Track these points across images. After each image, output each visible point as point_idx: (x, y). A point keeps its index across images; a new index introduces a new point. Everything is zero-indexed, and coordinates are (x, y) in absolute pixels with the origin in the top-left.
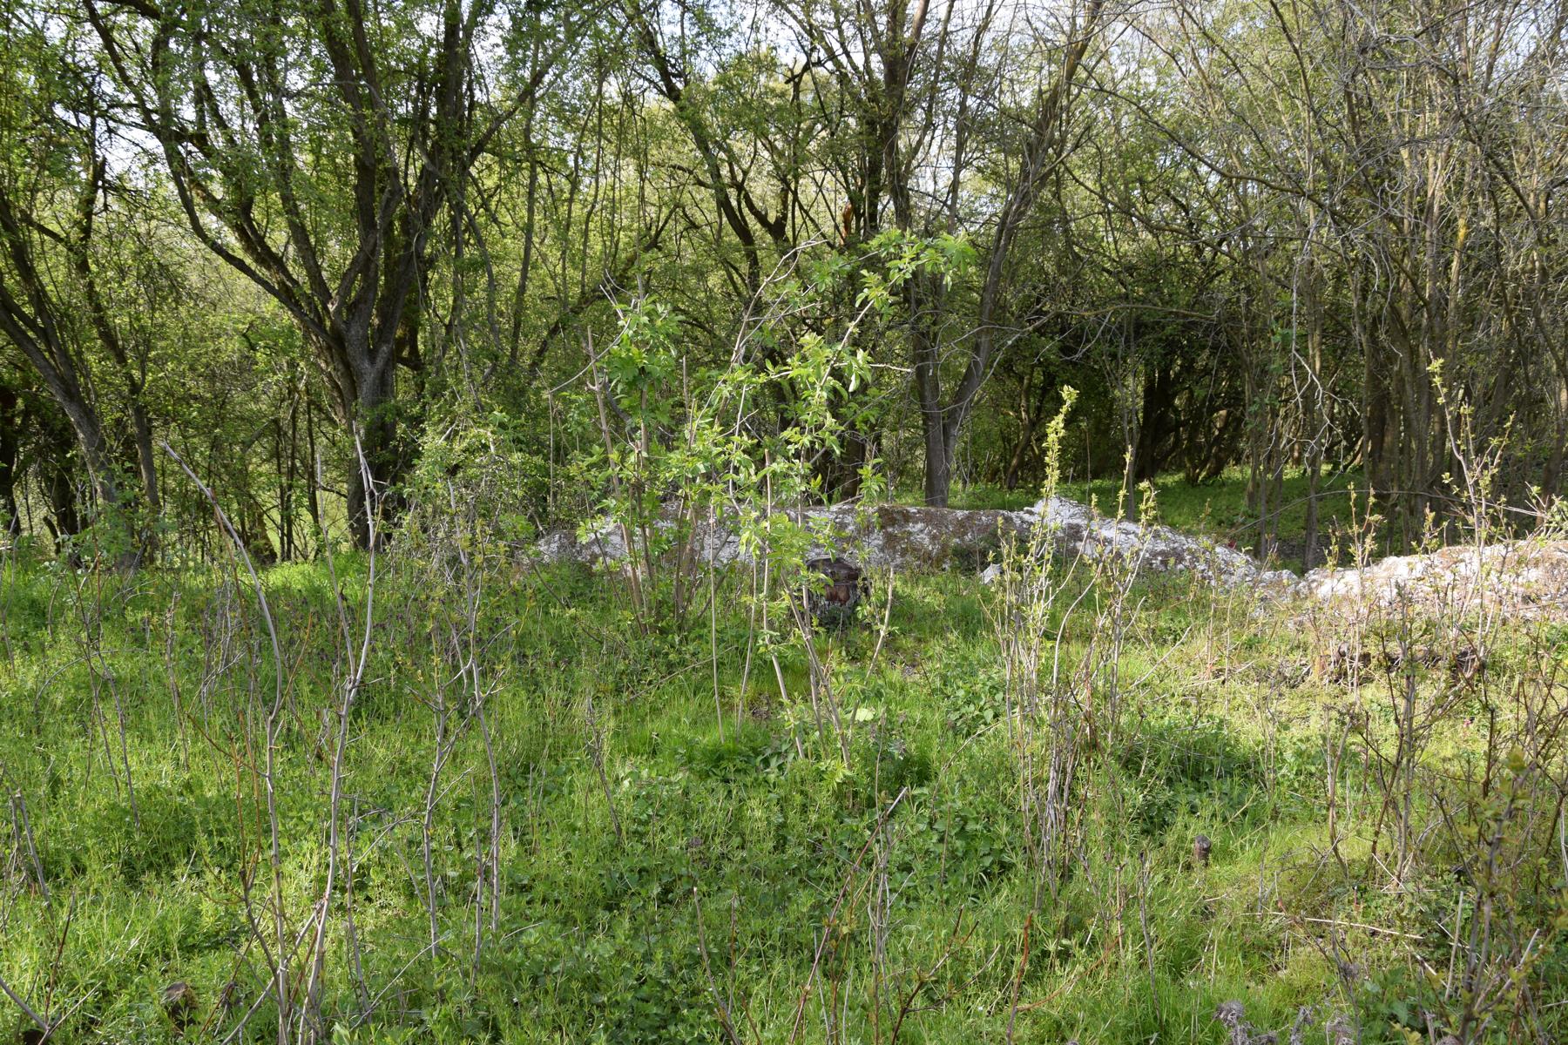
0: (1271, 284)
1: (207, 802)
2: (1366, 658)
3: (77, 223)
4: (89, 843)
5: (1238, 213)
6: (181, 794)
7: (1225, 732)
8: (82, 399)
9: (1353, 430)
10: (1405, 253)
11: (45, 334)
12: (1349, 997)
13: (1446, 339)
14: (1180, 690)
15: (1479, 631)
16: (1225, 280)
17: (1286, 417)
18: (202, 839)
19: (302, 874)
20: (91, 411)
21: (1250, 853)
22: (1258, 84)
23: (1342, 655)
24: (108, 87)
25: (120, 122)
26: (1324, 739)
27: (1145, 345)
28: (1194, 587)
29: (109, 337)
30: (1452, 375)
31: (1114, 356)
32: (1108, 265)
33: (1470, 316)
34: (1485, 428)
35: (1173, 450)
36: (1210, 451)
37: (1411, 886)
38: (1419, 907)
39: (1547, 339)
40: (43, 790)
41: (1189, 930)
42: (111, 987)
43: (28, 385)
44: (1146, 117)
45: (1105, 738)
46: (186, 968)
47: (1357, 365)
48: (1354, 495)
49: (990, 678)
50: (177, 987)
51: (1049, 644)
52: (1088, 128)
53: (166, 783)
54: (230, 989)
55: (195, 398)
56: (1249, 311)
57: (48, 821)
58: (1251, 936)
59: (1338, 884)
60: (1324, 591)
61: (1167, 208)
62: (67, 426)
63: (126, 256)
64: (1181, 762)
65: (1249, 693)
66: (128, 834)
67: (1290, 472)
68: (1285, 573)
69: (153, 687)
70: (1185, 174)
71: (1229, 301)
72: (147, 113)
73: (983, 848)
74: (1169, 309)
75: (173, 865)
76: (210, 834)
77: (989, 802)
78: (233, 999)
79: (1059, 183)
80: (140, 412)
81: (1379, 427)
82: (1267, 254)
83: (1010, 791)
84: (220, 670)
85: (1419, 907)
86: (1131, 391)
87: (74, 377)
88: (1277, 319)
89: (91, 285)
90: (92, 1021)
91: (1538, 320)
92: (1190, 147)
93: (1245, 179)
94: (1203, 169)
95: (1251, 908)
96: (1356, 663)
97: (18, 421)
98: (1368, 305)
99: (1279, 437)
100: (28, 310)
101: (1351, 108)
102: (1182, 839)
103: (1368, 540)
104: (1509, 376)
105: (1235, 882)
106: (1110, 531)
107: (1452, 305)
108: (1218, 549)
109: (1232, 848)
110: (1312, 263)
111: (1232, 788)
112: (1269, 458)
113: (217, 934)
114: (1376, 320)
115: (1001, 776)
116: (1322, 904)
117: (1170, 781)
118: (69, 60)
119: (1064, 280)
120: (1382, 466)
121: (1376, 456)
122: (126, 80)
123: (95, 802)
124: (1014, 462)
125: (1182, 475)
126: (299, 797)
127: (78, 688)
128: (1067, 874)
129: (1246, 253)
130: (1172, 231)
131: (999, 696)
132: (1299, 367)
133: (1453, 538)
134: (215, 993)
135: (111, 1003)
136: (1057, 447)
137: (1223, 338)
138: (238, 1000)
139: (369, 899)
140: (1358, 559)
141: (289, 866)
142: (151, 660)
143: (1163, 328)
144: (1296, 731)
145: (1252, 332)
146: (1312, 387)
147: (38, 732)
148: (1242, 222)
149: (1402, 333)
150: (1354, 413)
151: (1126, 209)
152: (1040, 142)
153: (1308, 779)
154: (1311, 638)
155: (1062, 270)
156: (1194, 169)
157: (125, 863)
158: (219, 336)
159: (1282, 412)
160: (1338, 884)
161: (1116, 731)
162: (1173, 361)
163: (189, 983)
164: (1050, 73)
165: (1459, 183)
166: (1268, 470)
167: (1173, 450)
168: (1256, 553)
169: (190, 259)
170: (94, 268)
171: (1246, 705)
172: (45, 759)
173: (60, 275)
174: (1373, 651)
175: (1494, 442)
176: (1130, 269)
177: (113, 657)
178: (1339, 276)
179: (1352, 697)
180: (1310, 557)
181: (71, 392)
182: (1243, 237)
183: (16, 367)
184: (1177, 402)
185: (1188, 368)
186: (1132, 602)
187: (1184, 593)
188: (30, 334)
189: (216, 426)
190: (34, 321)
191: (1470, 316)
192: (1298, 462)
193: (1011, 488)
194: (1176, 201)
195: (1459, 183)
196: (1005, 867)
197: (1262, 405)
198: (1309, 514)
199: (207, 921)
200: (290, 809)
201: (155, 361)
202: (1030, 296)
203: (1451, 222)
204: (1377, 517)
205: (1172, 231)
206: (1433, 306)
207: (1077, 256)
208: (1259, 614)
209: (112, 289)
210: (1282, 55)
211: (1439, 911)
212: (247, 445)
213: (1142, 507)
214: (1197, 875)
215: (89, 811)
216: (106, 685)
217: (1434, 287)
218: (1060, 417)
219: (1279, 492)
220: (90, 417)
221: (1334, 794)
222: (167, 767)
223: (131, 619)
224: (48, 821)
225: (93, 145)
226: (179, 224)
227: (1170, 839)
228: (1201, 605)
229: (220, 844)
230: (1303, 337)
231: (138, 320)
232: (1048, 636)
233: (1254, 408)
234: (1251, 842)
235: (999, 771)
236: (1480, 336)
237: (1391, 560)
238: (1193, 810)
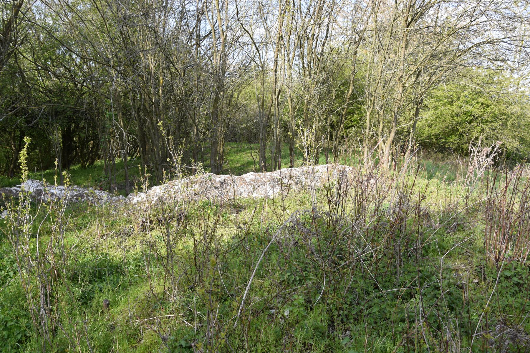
0: (103, 97)
2: (151, 222)
5: (88, 72)
7: (108, 258)
9: (135, 145)
10: (146, 87)
12: (166, 345)
13: (160, 115)
14: (90, 246)
15: (183, 206)
16: (87, 95)
17: (114, 142)
21: (124, 300)
22: (90, 27)
23: (144, 222)
26: (142, 252)
27: (60, 119)
28: (89, 207)
30: (165, 126)
31: (48, 124)
32: (41, 90)
33: (167, 107)
34: (177, 143)
35: (75, 156)
36: (89, 156)
37: (178, 297)
38: (182, 304)
41: (107, 337)
44: (50, 34)
45: (63, 272)
47: (134, 124)
48: (140, 168)
49: (10, 258)
51: (34, 240)
52: (26, 37)
56: (96, 106)
58: (130, 332)
59: (155, 303)
60: (135, 200)
61: (62, 69)
64: (94, 273)
65: (114, 241)
67: (117, 161)
68: (121, 197)
70: (67, 57)
71: (88, 103)
73: (16, 331)
74: (67, 106)
77: (16, 311)
79: (16, 57)
81: (144, 144)
82: (100, 87)
83: (25, 304)
85: (182, 304)
86: (57, 136)
88: (107, 109)
91: (186, 109)
92: (68, 47)
93: (90, 60)
94: (74, 56)
95: (127, 321)
96: (148, 224)
98: (136, 104)
99: (112, 149)
101: (123, 38)
102: (98, 302)
103: (146, 183)
104: (179, 126)
105: (121, 313)
106: (55, 190)
107: (161, 104)
108: (96, 191)
109: (117, 300)
110: (116, 90)
111: (114, 278)
112: (110, 157)
114: (139, 109)
115: (20, 299)
116: (152, 312)
117: (91, 282)
119: (22, 95)
120: (146, 156)
121: (144, 152)
124: (12, 166)
125: (80, 165)
128: (54, 331)
129: (93, 86)
130: (65, 77)
131: (15, 265)
132: (116, 125)
133: (172, 178)
136: (25, 162)
137: (88, 116)
140: (144, 189)
143: (66, 113)
144: (133, 252)
145: (99, 114)
146: (121, 132)
148: (90, 75)
149: (148, 113)
150: (135, 140)
151: (46, 69)
152: (6, 40)
153: (139, 270)
154: (132, 218)
155: (22, 92)
156: (70, 56)
159: (112, 140)
160: (155, 303)
161: (67, 269)
162: (71, 125)
164: (7, 14)
165: (159, 65)
166: (110, 161)
167: (75, 156)
168: (110, 190)
171: (114, 246)
174: (153, 219)
175: (180, 147)
176: (51, 91)
178: (125, 94)
179: (149, 236)
180: (128, 189)
182: (91, 80)
184: (74, 139)
185: (77, 127)
186: (66, 216)
187: (86, 209)
191: (167, 107)
192: (119, 157)
193: (12, 177)
194: (65, 67)
195: (159, 65)
196: (28, 338)
197: (105, 139)
198: (126, 175)
202: (10, 101)
203: (158, 78)
204: (148, 174)
205: (65, 77)
206: (156, 104)
207: (28, 86)
208: (113, 212)
210: (97, 18)
211: (188, 303)
213: (65, 181)
214: (106, 316)
217: (155, 99)
218: (25, 149)
219: (115, 168)
221: (149, 271)
227: (94, 304)
228: (93, 213)
230: (116, 115)
232: (34, 236)
233: (102, 140)
234: (123, 296)
235: (19, 297)
236: (170, 114)
237: (154, 187)
238: (101, 290)
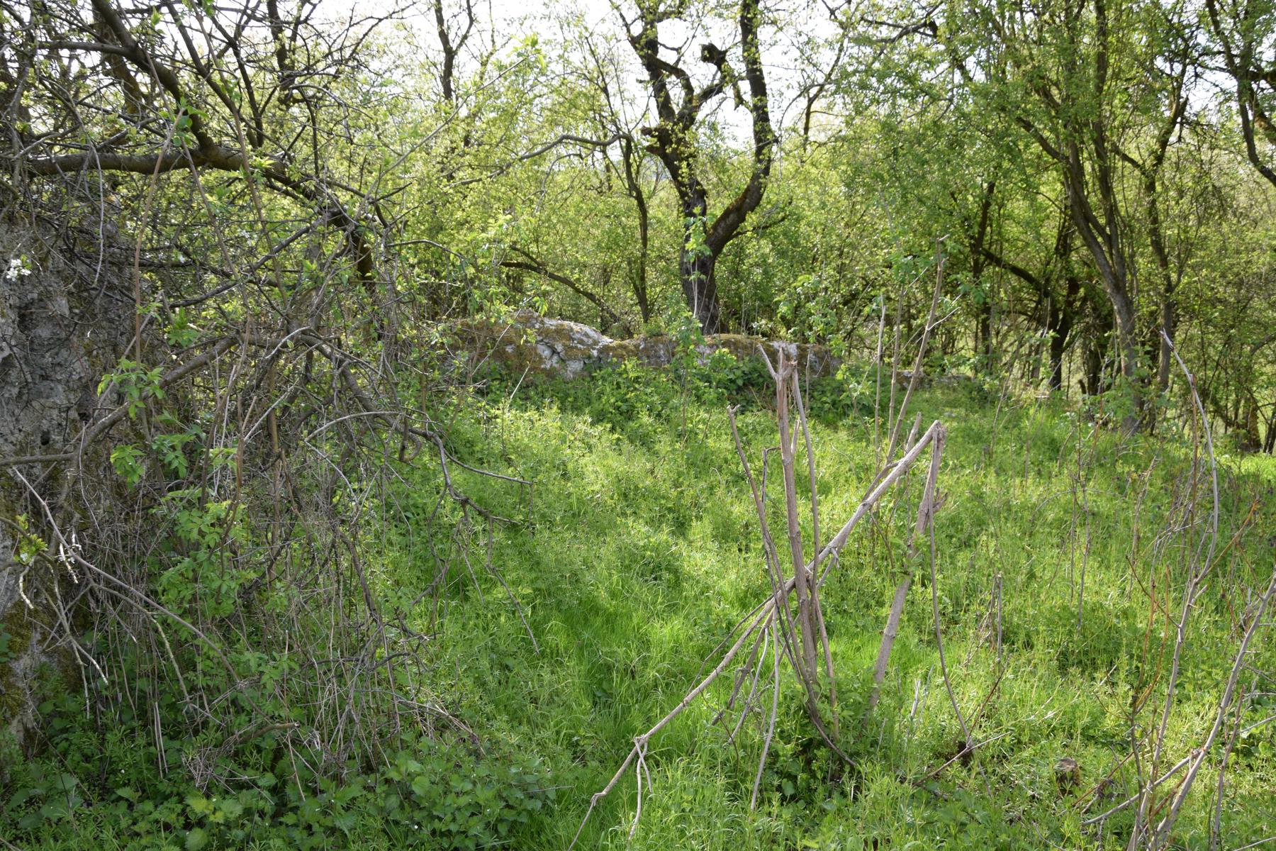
1: (1136, 630)
3: (1153, 152)
4: (1041, 628)
6: (1117, 617)
8: (1125, 293)
11: (1110, 240)
18: (1124, 658)
19: (1197, 720)
20: (1131, 303)
24: (1202, 39)
25: (1207, 67)
29: (1158, 246)
39: (816, 96)
40: (1021, 578)
42: (1025, 739)
43: (1090, 277)
46: (1082, 751)
50: (1070, 762)
53: (1108, 604)
54: (1104, 785)
55: (1220, 301)
57: (1017, 602)
62: (1111, 313)
63: (1188, 182)
66: (1070, 633)
69: (1121, 527)
72: (1230, 58)
75: (1096, 669)
76: (1132, 657)
78: (1106, 792)
80: (1170, 307)
84: (1177, 529)
87: (1124, 275)
89: (1154, 202)
90: (1005, 757)
97: (1078, 304)
100: (1102, 221)
113: (1113, 737)
118: (1175, 20)
122: (1219, 33)
123: (1053, 600)
126: (1213, 656)
127: (1066, 511)
134: (1096, 780)
135: (1020, 750)
138: (1111, 795)
139: (1250, 767)
141: (1187, 708)
142: (1124, 505)
147: (1031, 535)
157: (1062, 653)
158: (1254, 250)
163: (1079, 764)
169: (1240, 182)
170: (1159, 188)
172: (1029, 556)
173: (1131, 195)
177: (1096, 494)
181: (1119, 286)
183: (1085, 263)
188: (1100, 239)
189: (1232, 327)
190: (1104, 229)
199: (1109, 723)
200: (1203, 662)
201: (1193, 267)
209: (1170, 204)
212: (1257, 346)
215: (1047, 605)
216: (1089, 516)
220: (1128, 306)
222: (1114, 593)
223: (1119, 470)
224: (1017, 602)
225: (1180, 88)
226: (1239, 152)
229: (1137, 667)
231: (1186, 232)
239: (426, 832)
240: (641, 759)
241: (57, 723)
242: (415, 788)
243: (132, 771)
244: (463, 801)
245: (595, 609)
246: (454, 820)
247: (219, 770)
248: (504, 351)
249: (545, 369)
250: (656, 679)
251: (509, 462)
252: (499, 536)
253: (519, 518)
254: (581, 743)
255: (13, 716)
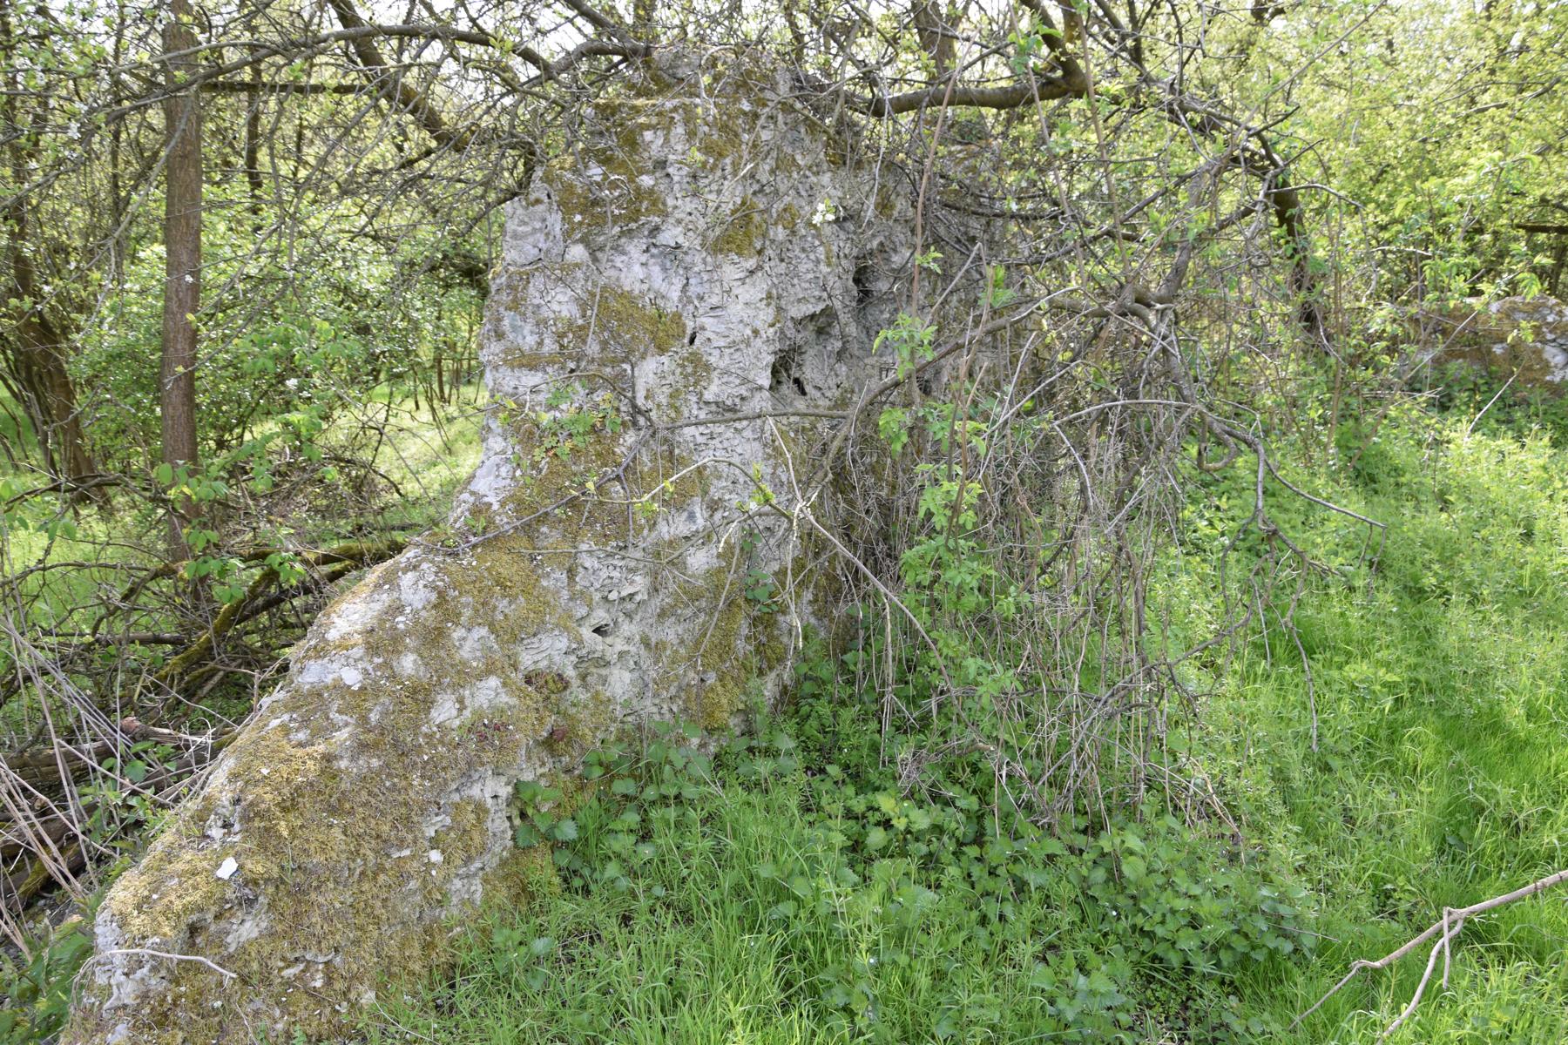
239: (1124, 924)
240: (1445, 939)
241: (808, 687)
242: (1126, 869)
243: (854, 752)
244: (1181, 904)
245: (1495, 726)
246: (1163, 923)
247: (925, 777)
248: (1489, 352)
249: (1551, 383)
250: (1554, 849)
251: (1445, 506)
252: (1386, 599)
253: (1429, 581)
254: (1396, 895)
255: (771, 668)
